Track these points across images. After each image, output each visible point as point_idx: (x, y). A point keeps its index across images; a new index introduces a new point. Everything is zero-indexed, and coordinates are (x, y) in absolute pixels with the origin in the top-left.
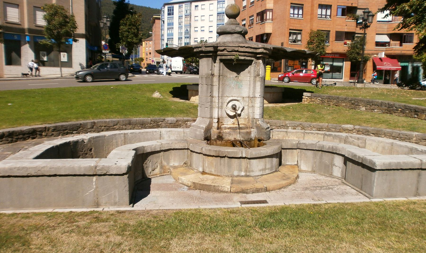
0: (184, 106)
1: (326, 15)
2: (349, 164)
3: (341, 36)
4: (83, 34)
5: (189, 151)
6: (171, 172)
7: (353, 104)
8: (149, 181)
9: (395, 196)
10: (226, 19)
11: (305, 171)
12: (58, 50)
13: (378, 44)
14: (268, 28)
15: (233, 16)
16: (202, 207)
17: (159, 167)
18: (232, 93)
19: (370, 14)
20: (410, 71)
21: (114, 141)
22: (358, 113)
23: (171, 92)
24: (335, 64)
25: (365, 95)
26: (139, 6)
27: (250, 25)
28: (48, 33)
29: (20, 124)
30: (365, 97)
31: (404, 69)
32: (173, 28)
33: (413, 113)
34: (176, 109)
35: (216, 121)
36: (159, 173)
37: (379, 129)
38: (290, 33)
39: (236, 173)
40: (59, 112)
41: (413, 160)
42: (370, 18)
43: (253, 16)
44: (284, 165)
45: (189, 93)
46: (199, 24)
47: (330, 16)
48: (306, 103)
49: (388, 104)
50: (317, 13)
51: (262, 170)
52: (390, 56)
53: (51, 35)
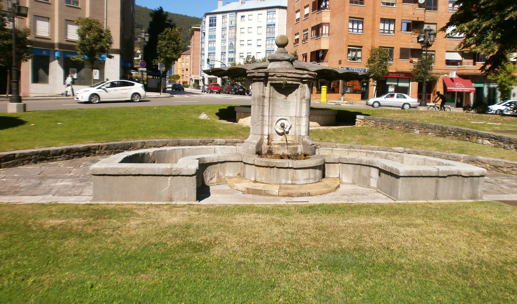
0: (233, 128)
1: (389, 30)
2: (382, 174)
3: (405, 53)
4: (117, 50)
5: (243, 163)
6: (226, 182)
7: (407, 127)
8: (208, 187)
9: (417, 200)
10: (276, 48)
11: (346, 183)
12: (91, 66)
13: (449, 62)
14: (324, 44)
15: (282, 46)
16: (255, 203)
17: (216, 177)
18: (280, 113)
19: (432, 32)
20: (486, 93)
21: (174, 155)
22: (411, 136)
23: (217, 114)
24: (401, 84)
25: (423, 118)
26: (174, 14)
27: (304, 40)
28: (81, 49)
29: (75, 142)
30: (423, 120)
31: (479, 91)
32: (215, 41)
33: (465, 136)
34: (225, 130)
35: (266, 137)
36: (216, 182)
37: (429, 151)
38: (349, 50)
39: (283, 181)
40: (109, 132)
41: (432, 169)
42: (432, 36)
43: (307, 30)
44: (327, 178)
45: (237, 115)
46: (246, 37)
47: (394, 31)
48: (359, 126)
49: (442, 127)
50: (379, 27)
51: (307, 179)
52: (463, 77)
53: (84, 51)
